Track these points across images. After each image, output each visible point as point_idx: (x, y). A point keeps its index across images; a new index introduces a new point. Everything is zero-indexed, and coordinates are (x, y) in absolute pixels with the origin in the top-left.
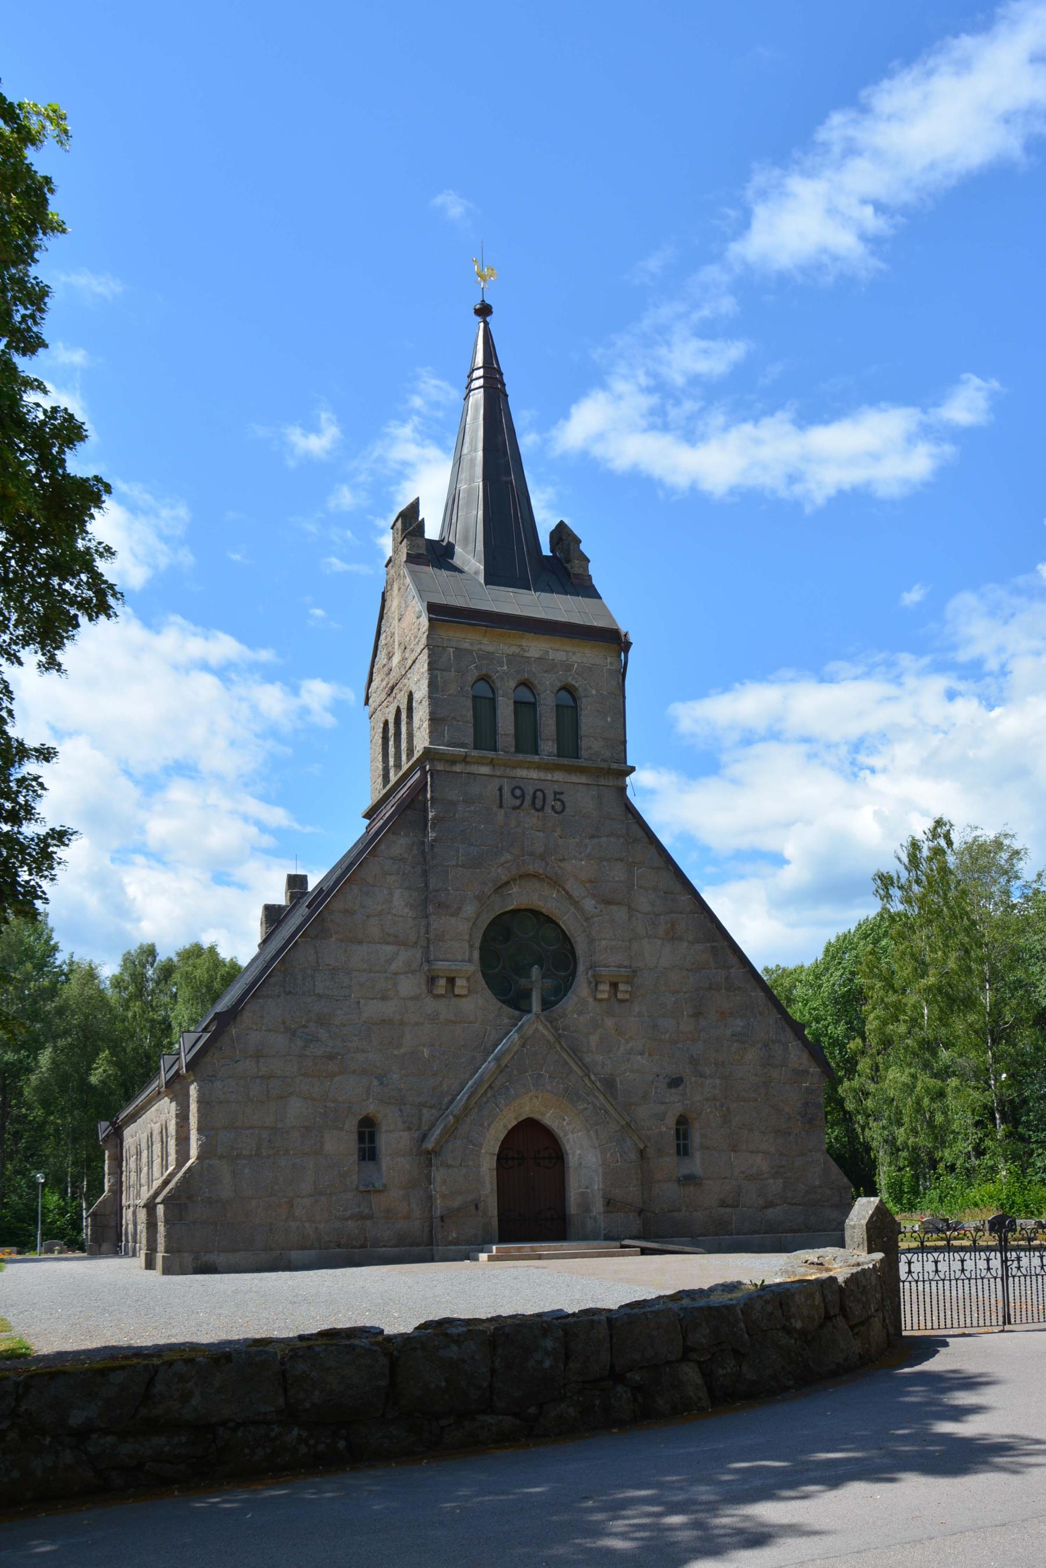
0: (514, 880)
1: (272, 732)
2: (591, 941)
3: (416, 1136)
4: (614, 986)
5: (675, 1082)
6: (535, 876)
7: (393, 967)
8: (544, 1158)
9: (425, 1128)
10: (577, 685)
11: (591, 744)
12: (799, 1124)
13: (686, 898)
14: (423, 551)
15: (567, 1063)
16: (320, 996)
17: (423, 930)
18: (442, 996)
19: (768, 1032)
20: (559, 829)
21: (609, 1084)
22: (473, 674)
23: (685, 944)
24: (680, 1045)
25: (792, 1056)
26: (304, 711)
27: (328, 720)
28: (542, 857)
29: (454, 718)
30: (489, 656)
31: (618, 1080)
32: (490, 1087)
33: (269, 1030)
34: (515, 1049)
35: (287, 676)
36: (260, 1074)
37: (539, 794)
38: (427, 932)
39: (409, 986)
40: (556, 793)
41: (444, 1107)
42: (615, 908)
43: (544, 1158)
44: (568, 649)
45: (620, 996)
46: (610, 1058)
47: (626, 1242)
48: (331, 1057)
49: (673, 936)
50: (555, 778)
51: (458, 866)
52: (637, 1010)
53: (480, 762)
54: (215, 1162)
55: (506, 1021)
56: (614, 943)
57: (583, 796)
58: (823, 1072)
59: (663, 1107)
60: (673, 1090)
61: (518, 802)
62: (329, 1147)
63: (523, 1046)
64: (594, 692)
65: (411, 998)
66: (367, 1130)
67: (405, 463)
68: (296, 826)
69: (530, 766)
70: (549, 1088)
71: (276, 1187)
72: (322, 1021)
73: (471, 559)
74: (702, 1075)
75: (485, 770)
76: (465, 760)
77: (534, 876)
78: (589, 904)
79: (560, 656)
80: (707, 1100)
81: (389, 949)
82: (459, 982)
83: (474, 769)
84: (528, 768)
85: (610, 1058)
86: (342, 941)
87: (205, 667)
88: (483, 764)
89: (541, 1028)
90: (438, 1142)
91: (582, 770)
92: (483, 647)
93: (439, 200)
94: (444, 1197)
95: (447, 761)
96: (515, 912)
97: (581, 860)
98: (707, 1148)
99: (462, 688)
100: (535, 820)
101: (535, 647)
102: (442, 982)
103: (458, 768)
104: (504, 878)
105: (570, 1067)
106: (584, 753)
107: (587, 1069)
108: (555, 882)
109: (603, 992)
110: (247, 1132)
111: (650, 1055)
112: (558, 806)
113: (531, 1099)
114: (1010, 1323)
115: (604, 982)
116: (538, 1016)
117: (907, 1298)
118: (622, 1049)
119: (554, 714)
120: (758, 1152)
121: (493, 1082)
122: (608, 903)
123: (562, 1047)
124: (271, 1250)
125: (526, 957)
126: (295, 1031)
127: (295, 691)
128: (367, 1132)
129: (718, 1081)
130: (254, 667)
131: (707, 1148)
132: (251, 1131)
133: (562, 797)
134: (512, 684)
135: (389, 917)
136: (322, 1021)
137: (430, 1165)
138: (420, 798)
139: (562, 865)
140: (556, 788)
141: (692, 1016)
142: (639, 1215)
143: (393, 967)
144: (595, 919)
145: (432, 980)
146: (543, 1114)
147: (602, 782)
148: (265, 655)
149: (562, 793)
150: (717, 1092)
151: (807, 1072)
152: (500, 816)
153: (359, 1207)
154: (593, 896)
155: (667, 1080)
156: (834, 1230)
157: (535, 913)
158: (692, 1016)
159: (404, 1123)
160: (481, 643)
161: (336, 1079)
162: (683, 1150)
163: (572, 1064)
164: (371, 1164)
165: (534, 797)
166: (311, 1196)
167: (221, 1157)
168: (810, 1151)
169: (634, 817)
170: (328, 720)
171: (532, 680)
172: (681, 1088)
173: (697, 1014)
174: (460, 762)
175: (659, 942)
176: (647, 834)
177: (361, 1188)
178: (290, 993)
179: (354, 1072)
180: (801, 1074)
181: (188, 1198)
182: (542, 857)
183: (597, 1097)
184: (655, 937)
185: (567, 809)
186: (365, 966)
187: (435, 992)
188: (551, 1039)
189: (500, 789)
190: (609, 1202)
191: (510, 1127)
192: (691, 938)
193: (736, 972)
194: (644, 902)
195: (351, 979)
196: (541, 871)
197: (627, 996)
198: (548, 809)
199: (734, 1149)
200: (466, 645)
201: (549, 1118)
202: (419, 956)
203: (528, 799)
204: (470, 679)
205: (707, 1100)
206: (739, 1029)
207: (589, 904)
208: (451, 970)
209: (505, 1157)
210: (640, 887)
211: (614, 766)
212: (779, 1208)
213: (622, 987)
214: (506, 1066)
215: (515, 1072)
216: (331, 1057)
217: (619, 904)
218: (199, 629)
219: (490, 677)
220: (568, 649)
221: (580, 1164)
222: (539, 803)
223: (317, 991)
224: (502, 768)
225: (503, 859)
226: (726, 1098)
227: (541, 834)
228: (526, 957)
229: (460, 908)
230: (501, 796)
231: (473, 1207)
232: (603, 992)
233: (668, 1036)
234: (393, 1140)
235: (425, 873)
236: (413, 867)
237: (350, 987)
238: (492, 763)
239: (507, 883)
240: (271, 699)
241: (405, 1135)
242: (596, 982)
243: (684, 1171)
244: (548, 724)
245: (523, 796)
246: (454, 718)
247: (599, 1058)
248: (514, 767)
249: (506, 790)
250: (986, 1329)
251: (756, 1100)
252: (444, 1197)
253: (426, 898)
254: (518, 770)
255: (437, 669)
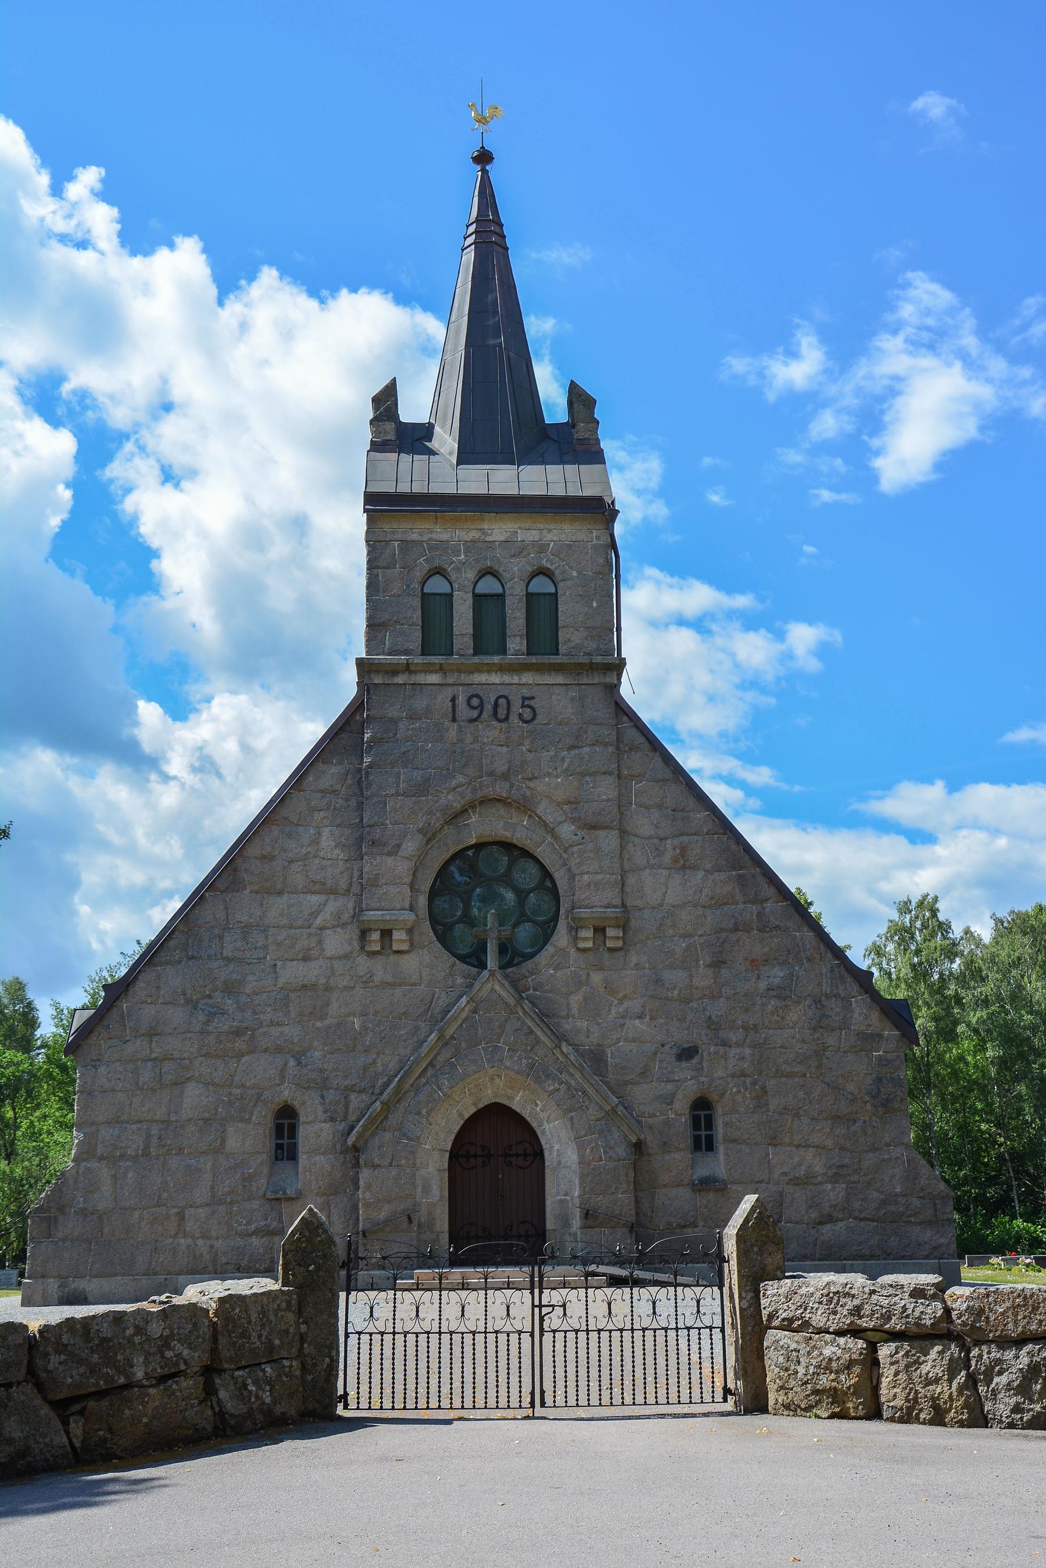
0: (474, 807)
1: (751, 683)
2: (572, 877)
3: (341, 1128)
4: (600, 931)
5: (687, 1053)
6: (499, 800)
7: (319, 921)
8: (517, 1155)
9: (352, 1118)
10: (552, 568)
11: (572, 637)
12: (869, 1107)
13: (702, 815)
14: (392, 436)
15: (532, 1032)
16: (229, 960)
17: (356, 874)
18: (378, 953)
19: (819, 984)
20: (527, 742)
21: (596, 1059)
22: (422, 566)
23: (701, 874)
24: (694, 1004)
25: (856, 1015)
26: (788, 656)
27: (813, 665)
28: (505, 777)
29: (396, 622)
30: (442, 546)
31: (609, 1052)
32: (431, 1064)
33: (167, 1003)
34: (464, 1015)
35: (766, 621)
36: (153, 1056)
37: (502, 701)
38: (361, 877)
39: (336, 942)
40: (524, 699)
41: (377, 1091)
42: (602, 833)
43: (517, 1155)
44: (542, 526)
45: (610, 944)
46: (598, 1024)
47: (593, 1268)
48: (238, 1032)
49: (683, 864)
50: (524, 681)
51: (398, 794)
52: (634, 960)
53: (428, 669)
54: (94, 1164)
55: (460, 981)
56: (599, 877)
57: (558, 699)
58: (903, 1035)
59: (670, 1087)
60: (684, 1064)
61: (475, 713)
62: (233, 1143)
63: (475, 1011)
64: (575, 574)
65: (340, 958)
66: (286, 1122)
67: (897, 378)
68: (784, 786)
69: (490, 669)
70: (508, 1064)
71: (165, 1195)
72: (231, 989)
73: (446, 441)
74: (725, 1043)
75: (434, 678)
76: (408, 668)
77: (499, 801)
78: (567, 831)
79: (532, 536)
80: (733, 1076)
81: (315, 899)
82: (397, 935)
83: (420, 678)
84: (489, 672)
85: (598, 1024)
86: (257, 892)
87: (681, 622)
88: (432, 672)
89: (497, 988)
90: (360, 1135)
91: (558, 668)
92: (434, 536)
93: (919, 104)
94: (367, 1205)
95: (387, 672)
96: (479, 846)
97: (557, 777)
98: (734, 1141)
99: (408, 586)
100: (496, 733)
101: (499, 529)
102: (375, 936)
103: (400, 679)
104: (457, 806)
105: (537, 1037)
106: (562, 649)
107: (560, 1037)
108: (525, 806)
109: (586, 939)
110: (134, 1127)
111: (652, 1018)
112: (527, 714)
113: (492, 1079)
114: (543, 1404)
115: (586, 927)
116: (492, 974)
117: (352, 1357)
118: (613, 1011)
119: (523, 604)
120: (809, 1146)
121: (435, 1058)
122: (594, 827)
123: (525, 1012)
124: (155, 1274)
125: (488, 901)
126: (197, 1003)
127: (780, 635)
128: (285, 1123)
129: (748, 1051)
130: (731, 615)
131: (734, 1141)
132: (139, 1125)
133: (532, 703)
134: (471, 575)
135: (317, 861)
136: (231, 989)
137: (357, 1165)
138: (358, 718)
139: (532, 785)
140: (526, 692)
141: (709, 966)
142: (631, 1232)
143: (319, 921)
144: (575, 849)
145: (364, 934)
146: (511, 1098)
147: (585, 681)
148: (742, 601)
149: (533, 698)
150: (746, 1066)
151: (880, 1036)
152: (452, 732)
153: (266, 1219)
154: (573, 820)
155: (675, 1051)
156: (927, 1257)
157: (507, 846)
158: (709, 966)
159: (325, 1112)
160: (432, 532)
161: (244, 1059)
162: (703, 1142)
163: (539, 1033)
164: (288, 1165)
165: (496, 705)
166: (207, 1205)
167: (101, 1158)
168: (888, 1145)
169: (631, 720)
170: (813, 665)
171: (496, 567)
172: (695, 1061)
173: (717, 964)
174: (403, 672)
175: (665, 873)
176: (648, 739)
177: (269, 1195)
178: (193, 957)
179: (266, 1050)
180: (869, 1040)
181: (59, 1209)
182: (505, 777)
183: (571, 1075)
184: (660, 867)
185: (539, 717)
186: (285, 921)
187: (367, 948)
188: (511, 1001)
189: (453, 700)
190: (587, 1214)
191: (467, 1116)
192: (708, 866)
193: (774, 906)
194: (643, 824)
195: (267, 937)
196: (504, 795)
197: (620, 944)
198: (514, 719)
199: (773, 1141)
200: (415, 537)
201: (517, 1103)
202: (351, 905)
203: (488, 707)
204: (418, 574)
205: (733, 1076)
206: (777, 981)
207: (567, 831)
208: (384, 921)
209: (462, 1153)
210: (639, 805)
211: (598, 659)
212: (841, 1224)
213: (611, 932)
214: (452, 1037)
215: (463, 1045)
216: (238, 1032)
217: (606, 828)
218: (675, 580)
219: (445, 570)
220: (542, 526)
221: (559, 1163)
222: (502, 713)
223: (225, 953)
224: (456, 675)
225: (454, 783)
226: (760, 1073)
227: (505, 749)
228: (488, 901)
229: (399, 846)
230: (454, 706)
231: (405, 1218)
232: (586, 939)
233: (676, 992)
234: (315, 1132)
235: (360, 807)
236: (347, 800)
237: (265, 947)
238: (441, 669)
239: (464, 812)
240: (754, 650)
241: (327, 1126)
242: (575, 928)
243: (701, 1172)
244: (516, 618)
245: (481, 705)
246: (396, 622)
247: (582, 1024)
248: (471, 672)
249: (461, 700)
250: (485, 1413)
251: (804, 1075)
252: (367, 1205)
253: (361, 838)
254: (476, 675)
255: (378, 567)
